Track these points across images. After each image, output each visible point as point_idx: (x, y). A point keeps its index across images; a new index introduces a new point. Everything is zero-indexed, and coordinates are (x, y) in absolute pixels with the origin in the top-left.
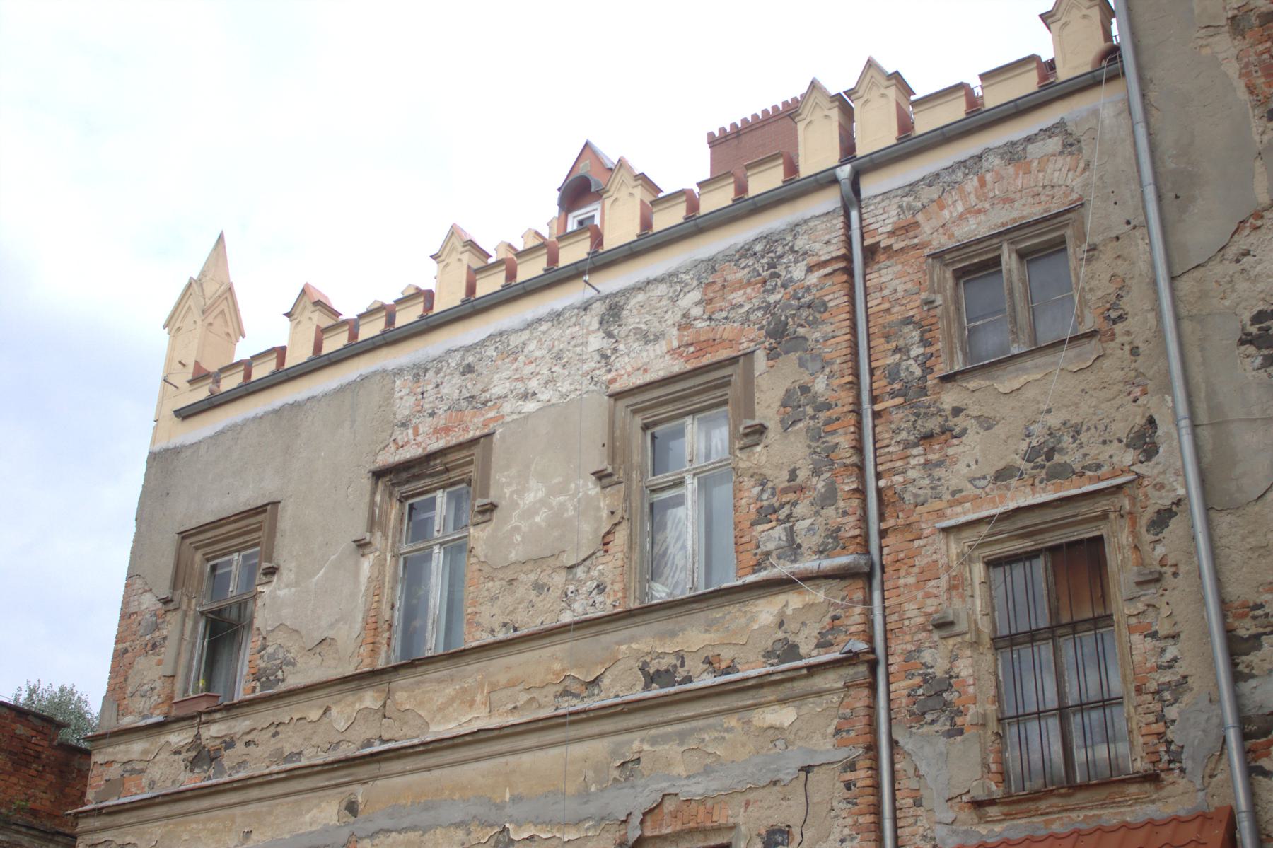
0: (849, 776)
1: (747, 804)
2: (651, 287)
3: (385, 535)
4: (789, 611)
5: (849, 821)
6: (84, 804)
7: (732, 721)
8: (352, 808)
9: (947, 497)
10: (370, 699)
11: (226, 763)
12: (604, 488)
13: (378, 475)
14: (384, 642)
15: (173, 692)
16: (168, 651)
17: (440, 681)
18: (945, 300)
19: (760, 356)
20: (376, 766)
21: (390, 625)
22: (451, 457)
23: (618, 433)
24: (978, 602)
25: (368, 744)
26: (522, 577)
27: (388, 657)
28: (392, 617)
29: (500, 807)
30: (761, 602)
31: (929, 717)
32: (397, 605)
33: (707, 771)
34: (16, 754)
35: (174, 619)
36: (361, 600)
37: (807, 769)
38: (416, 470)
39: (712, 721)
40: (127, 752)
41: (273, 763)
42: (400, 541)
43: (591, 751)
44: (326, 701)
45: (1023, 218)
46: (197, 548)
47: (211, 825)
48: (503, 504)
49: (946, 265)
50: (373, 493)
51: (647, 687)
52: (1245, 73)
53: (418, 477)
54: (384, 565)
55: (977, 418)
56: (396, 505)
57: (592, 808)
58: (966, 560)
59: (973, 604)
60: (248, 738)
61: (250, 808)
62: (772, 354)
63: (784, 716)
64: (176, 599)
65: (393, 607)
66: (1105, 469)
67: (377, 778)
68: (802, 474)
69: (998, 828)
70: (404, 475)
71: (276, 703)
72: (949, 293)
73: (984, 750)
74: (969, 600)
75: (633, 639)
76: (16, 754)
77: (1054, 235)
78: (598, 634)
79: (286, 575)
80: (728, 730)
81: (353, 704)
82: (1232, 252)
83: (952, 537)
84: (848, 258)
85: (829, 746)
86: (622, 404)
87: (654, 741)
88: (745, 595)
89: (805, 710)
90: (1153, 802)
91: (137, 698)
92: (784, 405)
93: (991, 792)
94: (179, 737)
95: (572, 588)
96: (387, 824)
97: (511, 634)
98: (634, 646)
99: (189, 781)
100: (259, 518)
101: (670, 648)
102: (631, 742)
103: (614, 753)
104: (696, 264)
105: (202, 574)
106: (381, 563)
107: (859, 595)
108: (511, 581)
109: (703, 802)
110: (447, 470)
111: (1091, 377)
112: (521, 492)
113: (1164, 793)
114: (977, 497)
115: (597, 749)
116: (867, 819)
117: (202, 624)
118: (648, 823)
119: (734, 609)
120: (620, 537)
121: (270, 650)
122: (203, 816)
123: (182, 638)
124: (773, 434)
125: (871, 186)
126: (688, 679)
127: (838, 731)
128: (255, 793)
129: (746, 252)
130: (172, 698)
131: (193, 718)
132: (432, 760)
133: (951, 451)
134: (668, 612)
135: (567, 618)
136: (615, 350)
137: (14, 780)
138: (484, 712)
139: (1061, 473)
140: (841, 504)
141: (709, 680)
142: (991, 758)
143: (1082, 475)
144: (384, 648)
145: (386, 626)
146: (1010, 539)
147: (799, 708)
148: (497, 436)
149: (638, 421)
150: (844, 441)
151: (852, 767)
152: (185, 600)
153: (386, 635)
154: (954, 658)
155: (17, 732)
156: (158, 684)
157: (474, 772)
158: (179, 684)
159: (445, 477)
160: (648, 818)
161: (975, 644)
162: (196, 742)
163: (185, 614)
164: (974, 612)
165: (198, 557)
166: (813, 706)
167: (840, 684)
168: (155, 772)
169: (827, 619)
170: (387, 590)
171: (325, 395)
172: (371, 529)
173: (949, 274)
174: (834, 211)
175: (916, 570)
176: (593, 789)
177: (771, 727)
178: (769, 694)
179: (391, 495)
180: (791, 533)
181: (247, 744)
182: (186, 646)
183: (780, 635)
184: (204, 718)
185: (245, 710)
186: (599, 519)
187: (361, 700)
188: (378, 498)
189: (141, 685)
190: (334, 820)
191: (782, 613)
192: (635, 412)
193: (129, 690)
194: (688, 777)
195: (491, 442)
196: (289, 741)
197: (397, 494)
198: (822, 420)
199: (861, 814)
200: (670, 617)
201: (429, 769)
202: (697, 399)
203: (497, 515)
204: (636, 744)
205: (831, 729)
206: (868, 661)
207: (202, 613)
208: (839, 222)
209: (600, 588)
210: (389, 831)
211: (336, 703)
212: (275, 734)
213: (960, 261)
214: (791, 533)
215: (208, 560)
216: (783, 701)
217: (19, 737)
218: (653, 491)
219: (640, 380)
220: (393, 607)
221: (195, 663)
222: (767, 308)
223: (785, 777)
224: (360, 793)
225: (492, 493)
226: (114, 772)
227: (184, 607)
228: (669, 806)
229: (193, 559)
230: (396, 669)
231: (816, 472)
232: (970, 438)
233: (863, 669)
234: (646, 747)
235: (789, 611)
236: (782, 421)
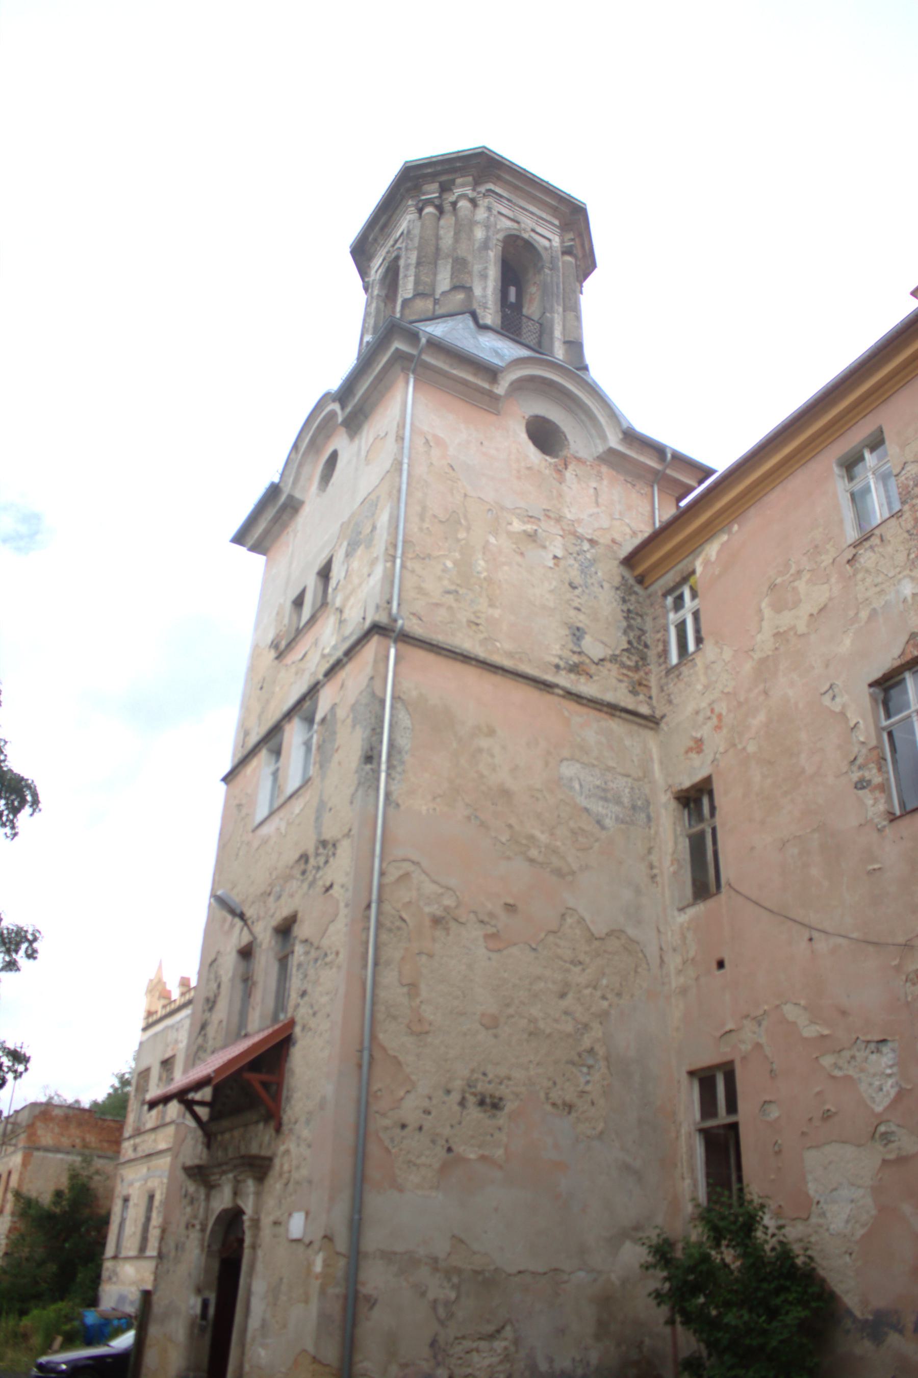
8: (149, 1169)
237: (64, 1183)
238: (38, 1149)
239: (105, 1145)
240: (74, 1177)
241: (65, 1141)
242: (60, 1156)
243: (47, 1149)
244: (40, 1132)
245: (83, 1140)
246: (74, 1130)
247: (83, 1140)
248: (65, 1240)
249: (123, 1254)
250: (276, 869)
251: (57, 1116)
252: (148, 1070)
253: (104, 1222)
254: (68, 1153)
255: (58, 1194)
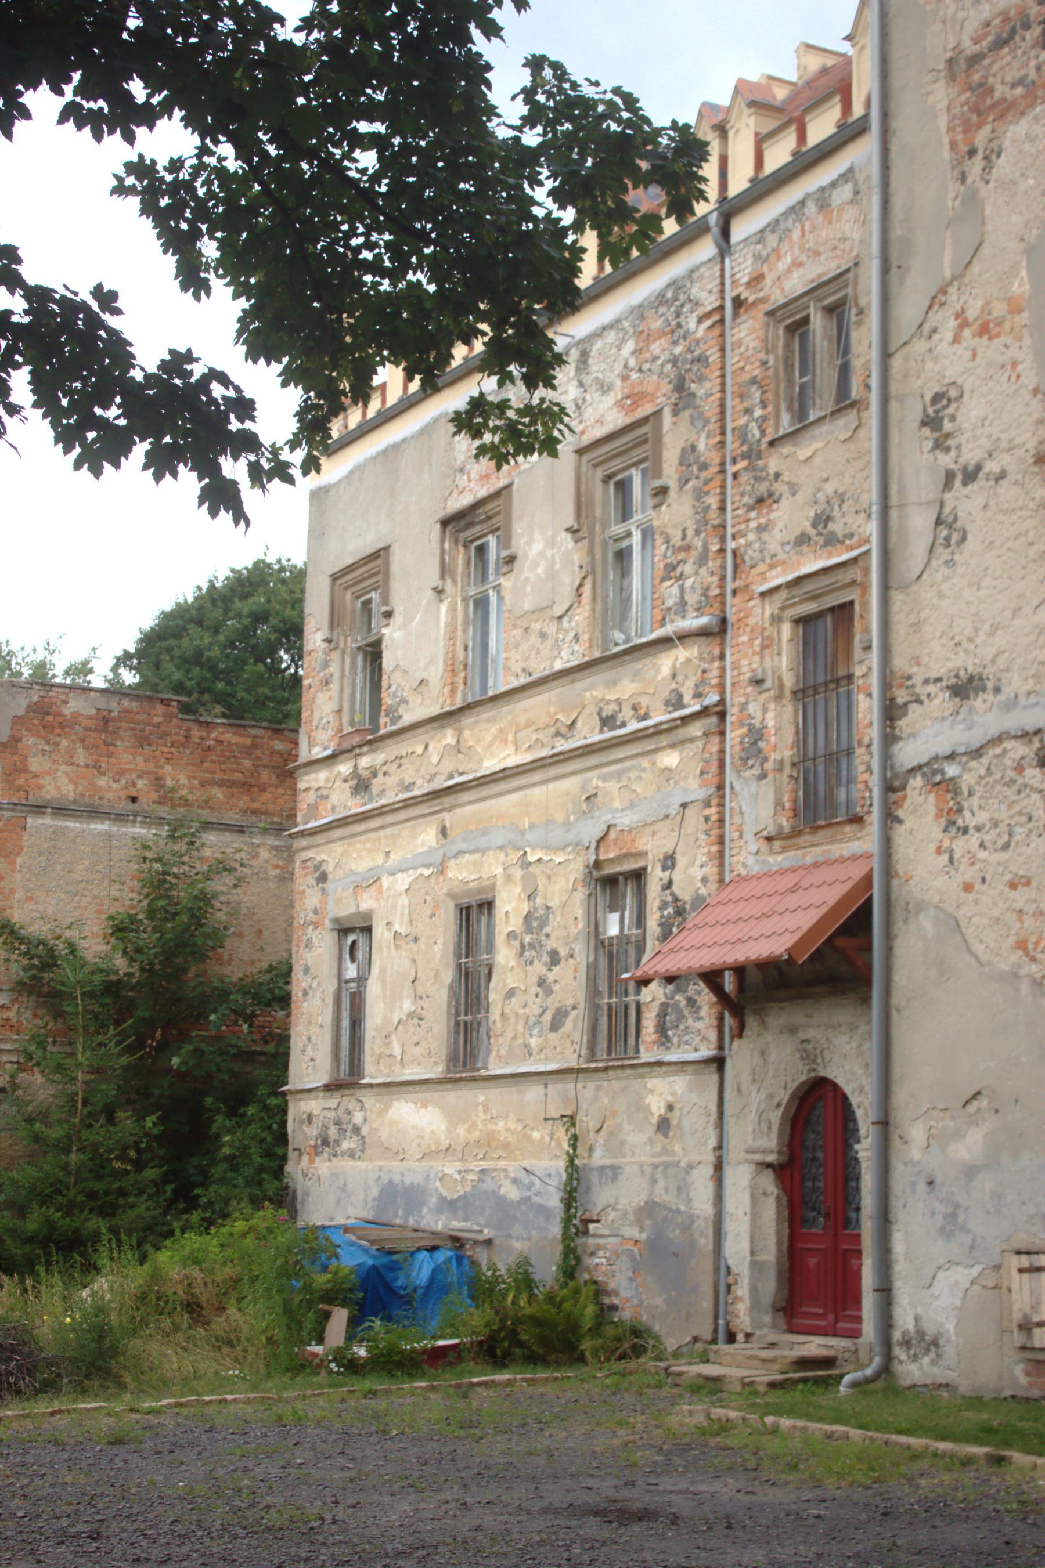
0: (707, 812)
1: (653, 834)
2: (606, 333)
3: (454, 581)
4: (678, 665)
5: (705, 850)
6: (296, 826)
7: (645, 763)
8: (444, 832)
9: (768, 560)
10: (449, 737)
11: (375, 790)
12: (576, 542)
13: (445, 523)
14: (461, 681)
15: (341, 724)
16: (335, 686)
17: (488, 721)
18: (776, 360)
19: (667, 412)
20: (454, 796)
21: (466, 666)
22: (490, 506)
23: (583, 489)
24: (784, 659)
25: (451, 777)
26: (533, 626)
27: (464, 694)
28: (466, 657)
29: (522, 833)
30: (663, 655)
31: (750, 763)
32: (470, 645)
33: (632, 805)
34: (278, 768)
35: (336, 656)
36: (442, 644)
37: (684, 805)
38: (468, 519)
39: (634, 762)
40: (317, 780)
41: (400, 791)
42: (469, 584)
43: (562, 790)
44: (425, 737)
45: (824, 274)
46: (346, 588)
47: (368, 845)
48: (520, 554)
49: (780, 321)
50: (442, 542)
51: (601, 731)
52: (950, 130)
53: (472, 524)
54: (455, 610)
55: (788, 483)
56: (462, 550)
57: (571, 836)
58: (777, 620)
59: (780, 661)
60: (384, 769)
61: (389, 831)
62: (675, 413)
63: (670, 759)
64: (335, 638)
65: (466, 648)
66: (856, 538)
67: (455, 806)
68: (690, 533)
69: (780, 858)
70: (463, 523)
71: (398, 738)
72: (780, 351)
73: (778, 792)
74: (776, 658)
75: (592, 687)
76: (278, 768)
77: (798, 317)
78: (573, 681)
79: (398, 618)
80: (644, 770)
81: (440, 741)
82: (926, 328)
83: (767, 601)
84: (721, 308)
85: (696, 786)
86: (586, 458)
87: (604, 778)
88: (649, 650)
89: (684, 754)
90: (858, 839)
91: (320, 731)
92: (681, 464)
93: (781, 827)
94: (344, 768)
95: (561, 637)
96: (462, 846)
97: (529, 679)
98: (594, 693)
99: (356, 806)
100: (380, 555)
101: (612, 697)
102: (591, 779)
103: (583, 788)
104: (633, 309)
105: (354, 611)
106: (453, 609)
107: (717, 652)
108: (527, 629)
109: (630, 831)
110: (489, 518)
111: (851, 446)
112: (529, 543)
113: (864, 832)
114: (784, 562)
115: (570, 785)
116: (714, 848)
117: (360, 658)
118: (602, 849)
119: (647, 661)
120: (587, 590)
121: (393, 688)
122: (362, 838)
123: (343, 675)
124: (672, 494)
125: (742, 229)
126: (624, 725)
127: (702, 773)
128: (390, 819)
129: (660, 299)
130: (341, 731)
131: (350, 750)
132: (485, 792)
133: (772, 516)
134: (610, 663)
135: (558, 666)
136: (584, 400)
137: (281, 791)
138: (511, 750)
139: (831, 541)
140: (710, 564)
141: (634, 726)
142: (786, 797)
143: (842, 542)
144: (461, 687)
145: (461, 667)
146: (801, 602)
147: (681, 752)
148: (515, 487)
149: (599, 474)
150: (713, 501)
151: (707, 804)
152: (342, 638)
153: (462, 675)
154: (765, 710)
155: (277, 748)
156: (331, 718)
157: (506, 803)
158: (346, 717)
159: (489, 523)
160: (602, 845)
161: (779, 698)
162: (355, 774)
163: (343, 652)
164: (780, 668)
165: (348, 596)
166: (690, 750)
167: (700, 733)
168: (335, 798)
169: (699, 673)
170: (460, 633)
171: (412, 437)
172: (443, 577)
173: (781, 332)
174: (710, 260)
175: (748, 629)
176: (572, 818)
177: (666, 769)
178: (664, 740)
179: (456, 542)
180: (682, 588)
181: (385, 774)
182: (347, 682)
183: (674, 686)
184: (357, 751)
185: (380, 744)
186: (573, 572)
187: (444, 737)
188: (447, 546)
189: (321, 719)
190: (434, 844)
191: (674, 666)
192: (596, 466)
193: (315, 723)
194: (623, 810)
195: (511, 493)
196: (408, 774)
197: (461, 540)
198: (702, 480)
199: (712, 844)
200: (612, 668)
201: (483, 799)
202: (634, 453)
203: (517, 565)
204: (594, 779)
205: (698, 772)
206: (717, 713)
207: (359, 649)
208: (717, 269)
209: (576, 638)
210: (464, 852)
211: (432, 738)
212: (400, 766)
213: (789, 317)
214: (682, 588)
215: (358, 598)
216: (672, 746)
217: (280, 754)
218: (616, 540)
219: (599, 432)
220: (466, 648)
221: (358, 695)
222: (674, 361)
223: (673, 811)
224: (447, 818)
225: (514, 543)
226: (311, 797)
227: (342, 645)
228: (612, 835)
229: (344, 599)
230: (461, 710)
231: (698, 532)
232: (784, 503)
233: (714, 719)
234: (600, 784)
235: (678, 665)
236: (680, 480)
237: (128, 898)
238: (39, 809)
239: (218, 793)
240: (158, 885)
241: (110, 789)
242: (100, 827)
243: (61, 810)
244: (35, 764)
245: (158, 782)
246: (126, 755)
247: (158, 782)
248: (164, 1047)
249: (373, 1073)
250: (1036, 118)
251: (76, 715)
252: (376, 562)
253: (272, 994)
254: (120, 818)
255: (121, 929)
